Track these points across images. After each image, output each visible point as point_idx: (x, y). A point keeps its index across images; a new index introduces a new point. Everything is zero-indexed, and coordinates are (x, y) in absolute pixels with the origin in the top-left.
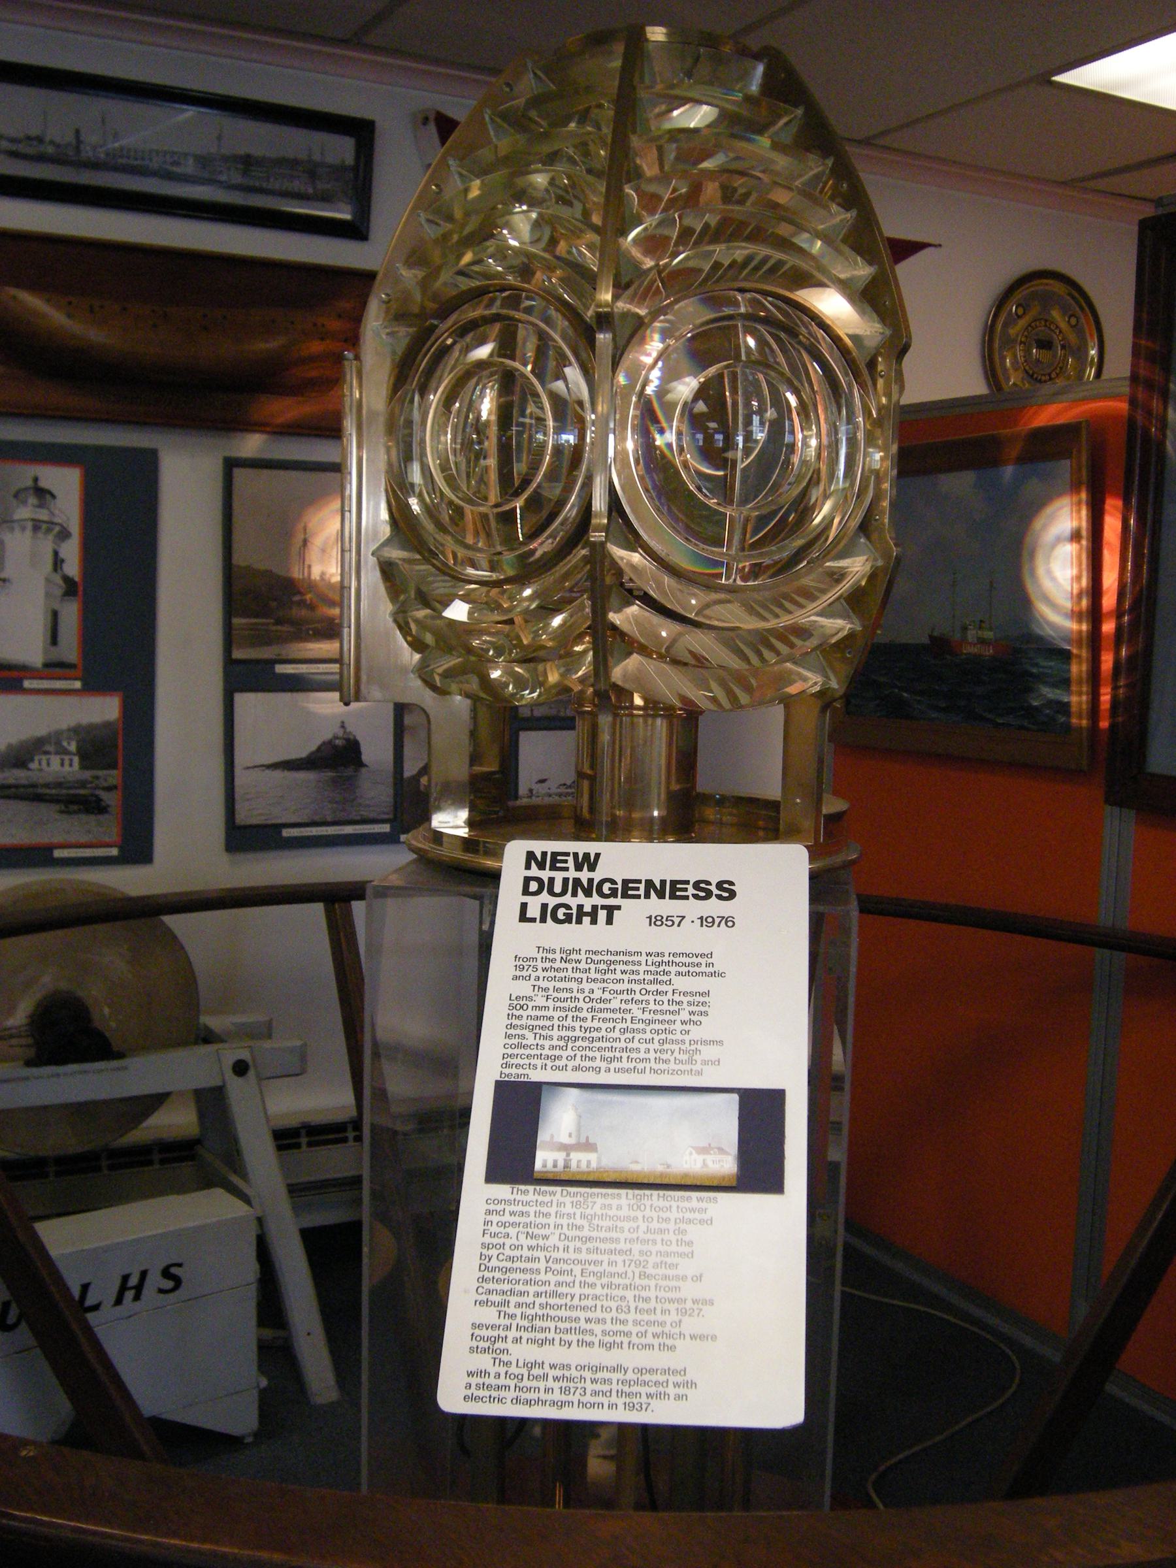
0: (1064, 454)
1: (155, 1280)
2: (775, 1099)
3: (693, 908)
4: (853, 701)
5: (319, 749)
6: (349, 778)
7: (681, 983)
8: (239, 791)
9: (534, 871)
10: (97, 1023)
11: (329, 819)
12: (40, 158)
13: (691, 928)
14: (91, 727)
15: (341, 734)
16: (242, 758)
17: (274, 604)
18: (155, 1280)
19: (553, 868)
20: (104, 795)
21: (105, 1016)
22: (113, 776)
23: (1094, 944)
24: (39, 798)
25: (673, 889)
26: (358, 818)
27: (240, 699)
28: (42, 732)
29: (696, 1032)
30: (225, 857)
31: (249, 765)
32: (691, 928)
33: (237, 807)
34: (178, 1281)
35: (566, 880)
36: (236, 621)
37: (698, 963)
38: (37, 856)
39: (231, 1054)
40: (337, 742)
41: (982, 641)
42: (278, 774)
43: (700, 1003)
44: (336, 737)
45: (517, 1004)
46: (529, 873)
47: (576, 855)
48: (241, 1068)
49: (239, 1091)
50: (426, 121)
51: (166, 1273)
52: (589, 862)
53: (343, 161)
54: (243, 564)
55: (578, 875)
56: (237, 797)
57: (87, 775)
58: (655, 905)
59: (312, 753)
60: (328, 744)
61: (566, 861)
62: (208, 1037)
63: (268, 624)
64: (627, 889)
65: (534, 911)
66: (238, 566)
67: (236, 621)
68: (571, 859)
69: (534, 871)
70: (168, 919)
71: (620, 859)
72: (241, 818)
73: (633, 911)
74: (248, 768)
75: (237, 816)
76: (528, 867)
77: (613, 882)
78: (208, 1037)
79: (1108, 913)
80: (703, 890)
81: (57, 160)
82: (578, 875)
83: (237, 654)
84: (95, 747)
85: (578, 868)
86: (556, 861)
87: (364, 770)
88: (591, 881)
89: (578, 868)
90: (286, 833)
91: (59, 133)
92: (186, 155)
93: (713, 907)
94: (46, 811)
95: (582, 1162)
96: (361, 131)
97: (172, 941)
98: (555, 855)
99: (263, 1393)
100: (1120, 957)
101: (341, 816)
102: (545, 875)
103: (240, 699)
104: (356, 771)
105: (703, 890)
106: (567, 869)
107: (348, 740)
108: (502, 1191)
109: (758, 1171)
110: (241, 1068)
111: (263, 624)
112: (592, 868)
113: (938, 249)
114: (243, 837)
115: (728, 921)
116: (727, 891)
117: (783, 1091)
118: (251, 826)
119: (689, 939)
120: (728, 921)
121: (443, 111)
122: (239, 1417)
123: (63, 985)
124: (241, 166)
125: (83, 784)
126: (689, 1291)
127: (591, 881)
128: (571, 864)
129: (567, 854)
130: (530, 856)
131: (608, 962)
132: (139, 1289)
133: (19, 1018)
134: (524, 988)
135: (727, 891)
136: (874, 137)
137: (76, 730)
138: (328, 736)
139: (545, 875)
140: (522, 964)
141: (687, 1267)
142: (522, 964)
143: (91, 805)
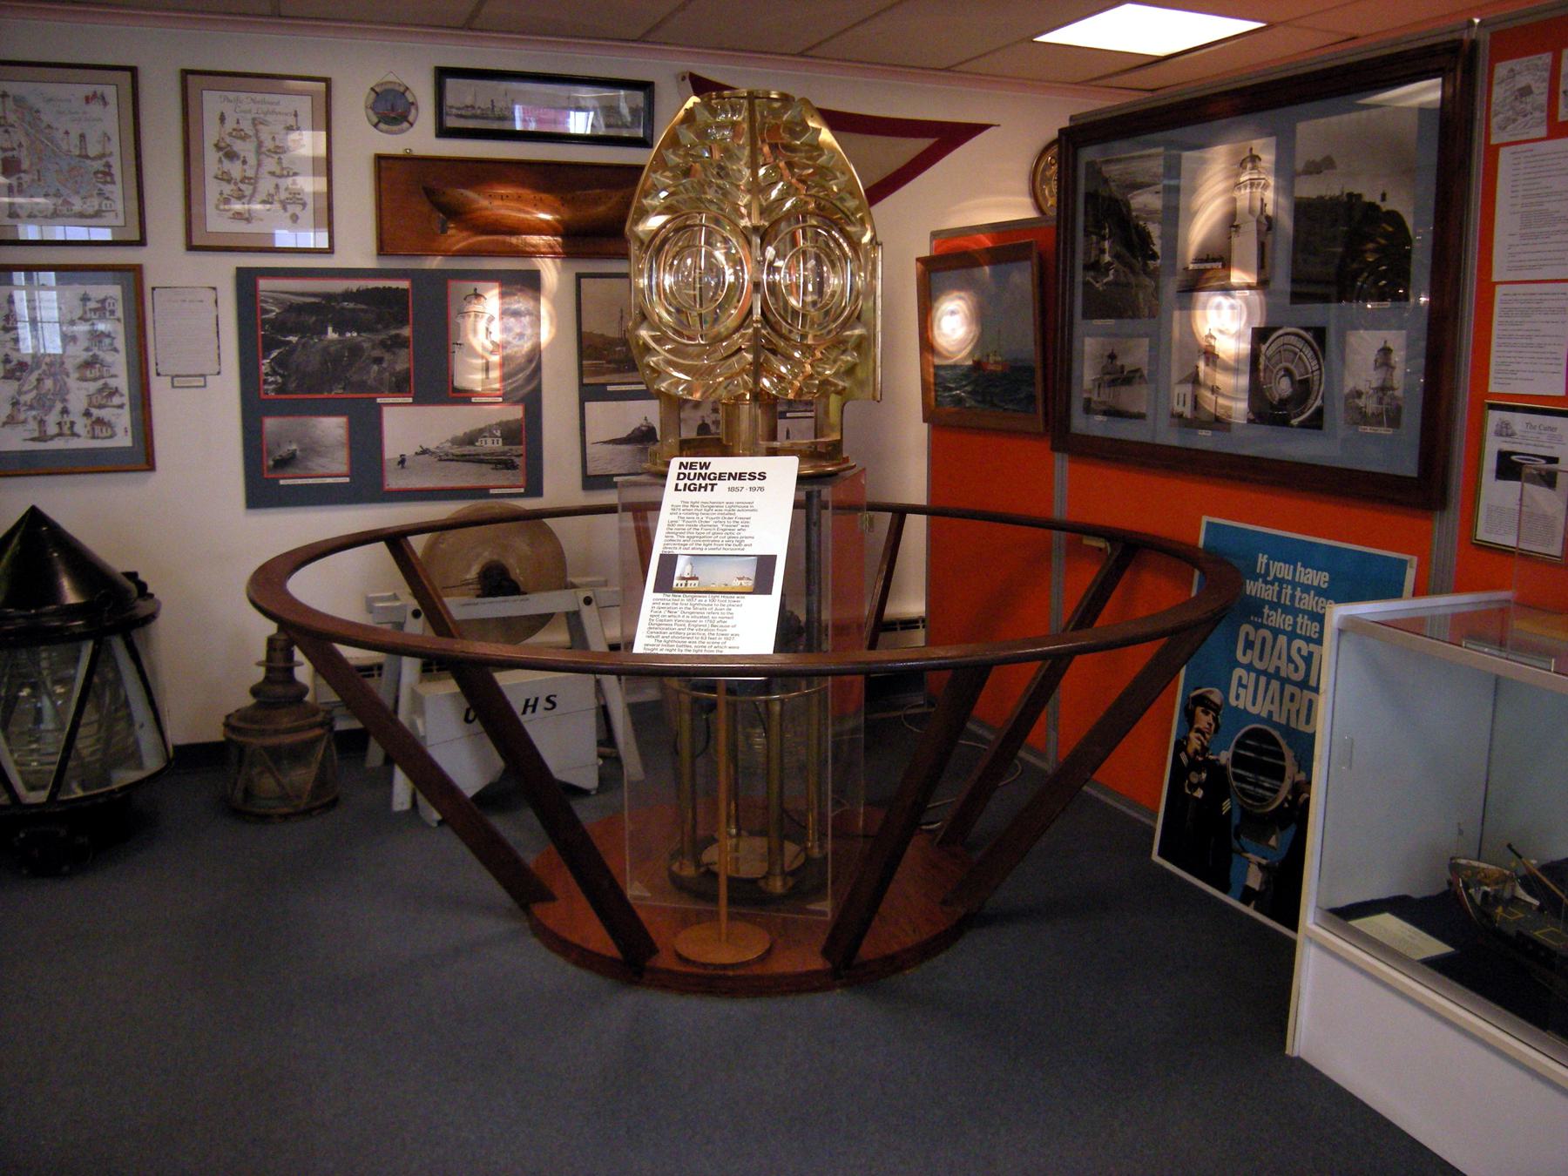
0: (1027, 258)
1: (542, 703)
2: (773, 558)
3: (747, 484)
7: (739, 514)
10: (513, 576)
12: (475, 117)
13: (746, 492)
14: (508, 422)
18: (542, 703)
20: (516, 460)
21: (517, 573)
22: (520, 449)
23: (1054, 528)
24: (481, 461)
25: (741, 476)
28: (482, 425)
29: (743, 534)
32: (746, 492)
34: (554, 705)
37: (748, 506)
38: (481, 492)
39: (582, 594)
41: (996, 363)
42: (610, 446)
43: (746, 522)
45: (671, 524)
48: (588, 601)
49: (589, 616)
50: (684, 79)
51: (548, 699)
52: (706, 466)
57: (507, 448)
58: (732, 483)
62: (574, 586)
64: (721, 477)
65: (681, 486)
70: (546, 520)
71: (718, 464)
72: (591, 471)
73: (722, 485)
78: (574, 586)
79: (1059, 512)
80: (752, 476)
81: (483, 117)
83: (586, 381)
84: (510, 433)
86: (692, 466)
91: (483, 103)
93: (756, 483)
94: (485, 468)
95: (692, 585)
96: (646, 87)
97: (550, 533)
99: (600, 768)
100: (1063, 534)
105: (752, 476)
108: (660, 595)
109: (762, 585)
110: (588, 601)
114: (592, 482)
115: (761, 489)
116: (763, 476)
117: (238, 269)
119: (745, 496)
120: (761, 489)
122: (589, 780)
123: (495, 557)
125: (504, 453)
126: (730, 631)
131: (710, 506)
132: (534, 707)
133: (473, 573)
134: (674, 518)
135: (763, 476)
137: (500, 425)
138: (637, 425)
140: (674, 508)
141: (730, 622)
142: (674, 508)
143: (509, 465)
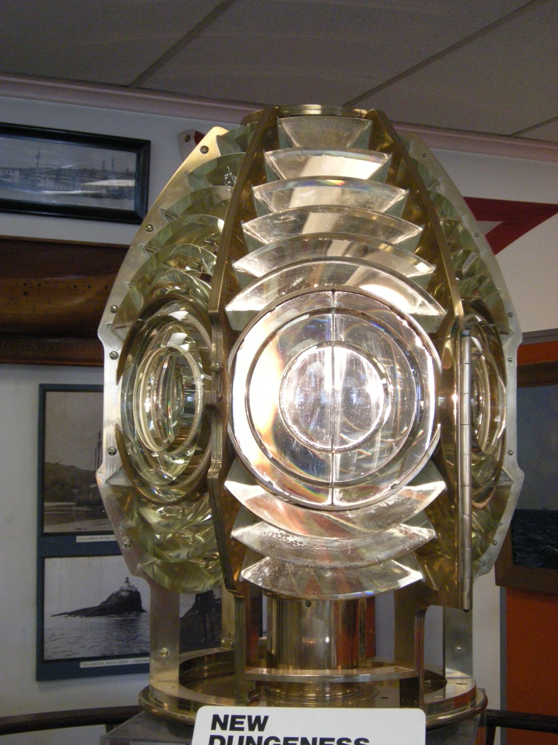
4: (519, 554)
5: (109, 599)
6: (132, 621)
8: (47, 635)
9: (218, 731)
11: (116, 653)
15: (125, 586)
16: (50, 608)
17: (75, 491)
19: (233, 728)
26: (139, 652)
27: (50, 563)
30: (36, 685)
31: (56, 614)
33: (46, 646)
35: (241, 738)
36: (47, 504)
40: (124, 594)
42: (78, 620)
44: (122, 590)
46: (214, 733)
47: (250, 718)
52: (259, 723)
53: (128, 169)
54: (53, 461)
55: (251, 734)
56: (46, 637)
59: (104, 602)
60: (116, 595)
61: (242, 723)
63: (71, 506)
66: (49, 464)
67: (47, 504)
68: (246, 721)
69: (218, 731)
72: (49, 654)
74: (54, 616)
75: (45, 653)
76: (214, 727)
77: (277, 739)
82: (251, 734)
83: (48, 529)
85: (252, 728)
87: (143, 614)
88: (260, 739)
89: (252, 728)
90: (83, 665)
92: (13, 170)
96: (140, 148)
98: (234, 717)
101: (126, 651)
102: (226, 734)
103: (50, 563)
104: (137, 615)
106: (242, 729)
107: (131, 592)
111: (67, 506)
112: (262, 728)
113: (52, 614)
114: (51, 669)
118: (57, 661)
121: (198, 131)
124: (54, 177)
127: (260, 739)
128: (246, 725)
129: (243, 717)
130: (216, 718)
136: (520, 132)
138: (116, 589)
139: (226, 734)
